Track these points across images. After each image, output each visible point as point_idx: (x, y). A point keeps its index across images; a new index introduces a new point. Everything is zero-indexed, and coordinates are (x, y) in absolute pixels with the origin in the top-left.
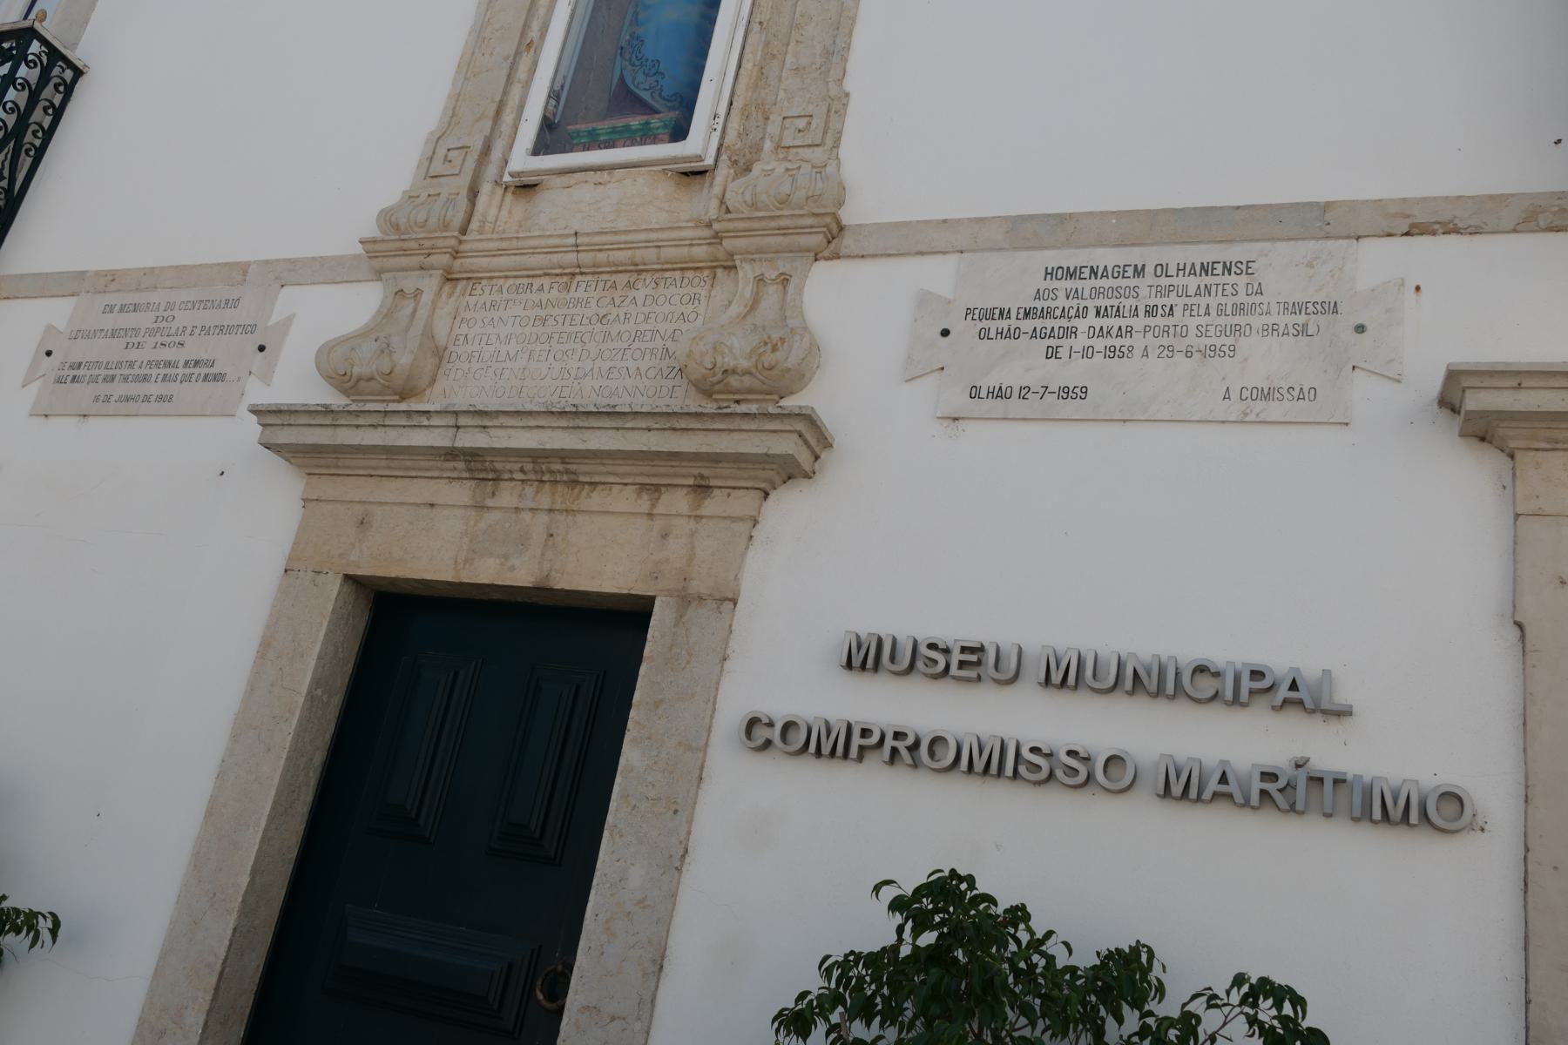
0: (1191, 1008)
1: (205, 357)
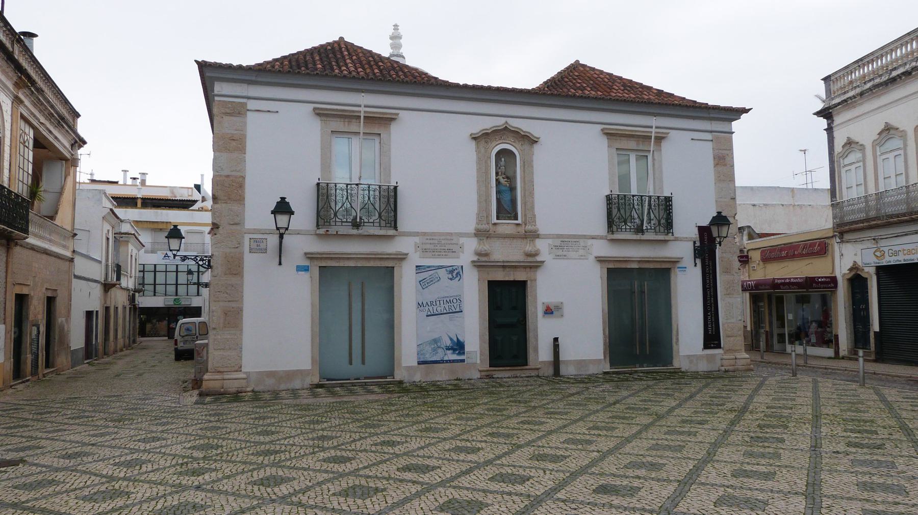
0: (751, 254)
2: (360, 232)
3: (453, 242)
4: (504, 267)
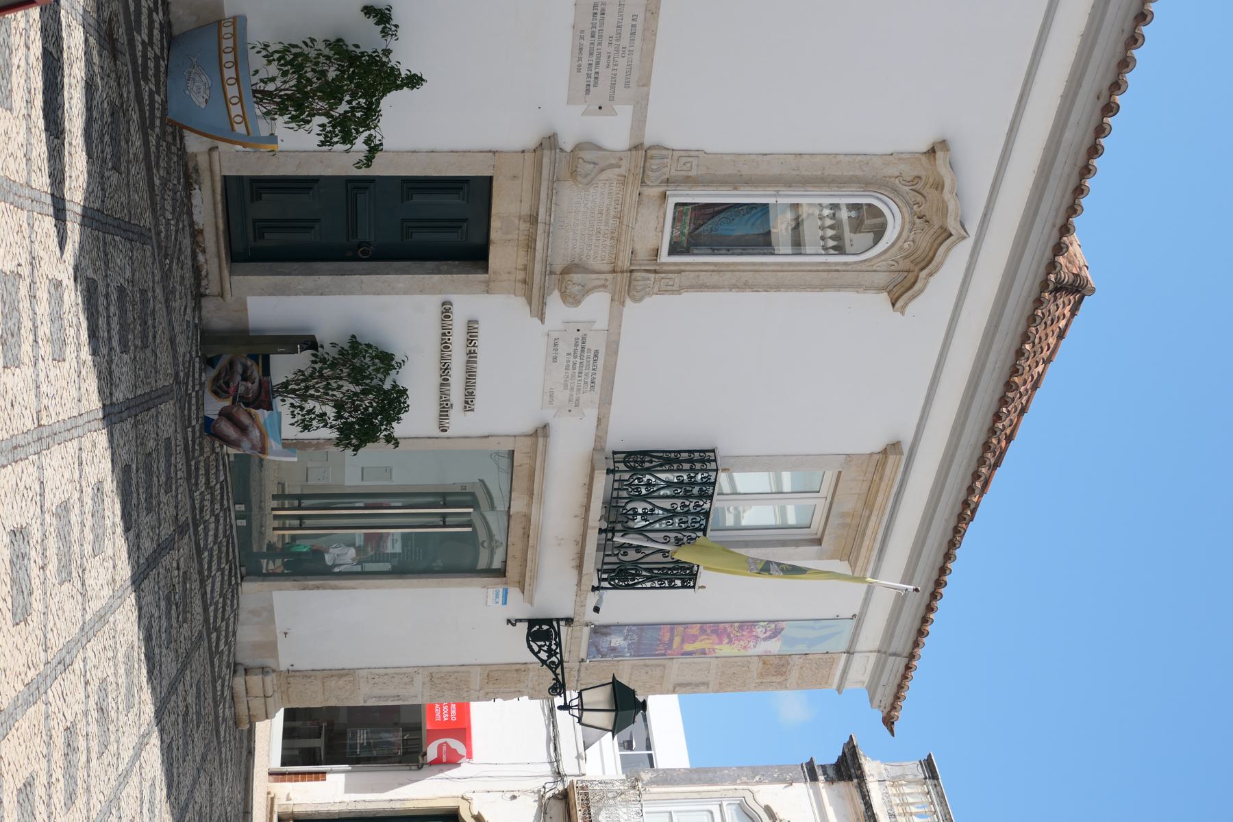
1: (600, 81)
2: (973, 228)
3: (620, 89)
4: (533, 219)
